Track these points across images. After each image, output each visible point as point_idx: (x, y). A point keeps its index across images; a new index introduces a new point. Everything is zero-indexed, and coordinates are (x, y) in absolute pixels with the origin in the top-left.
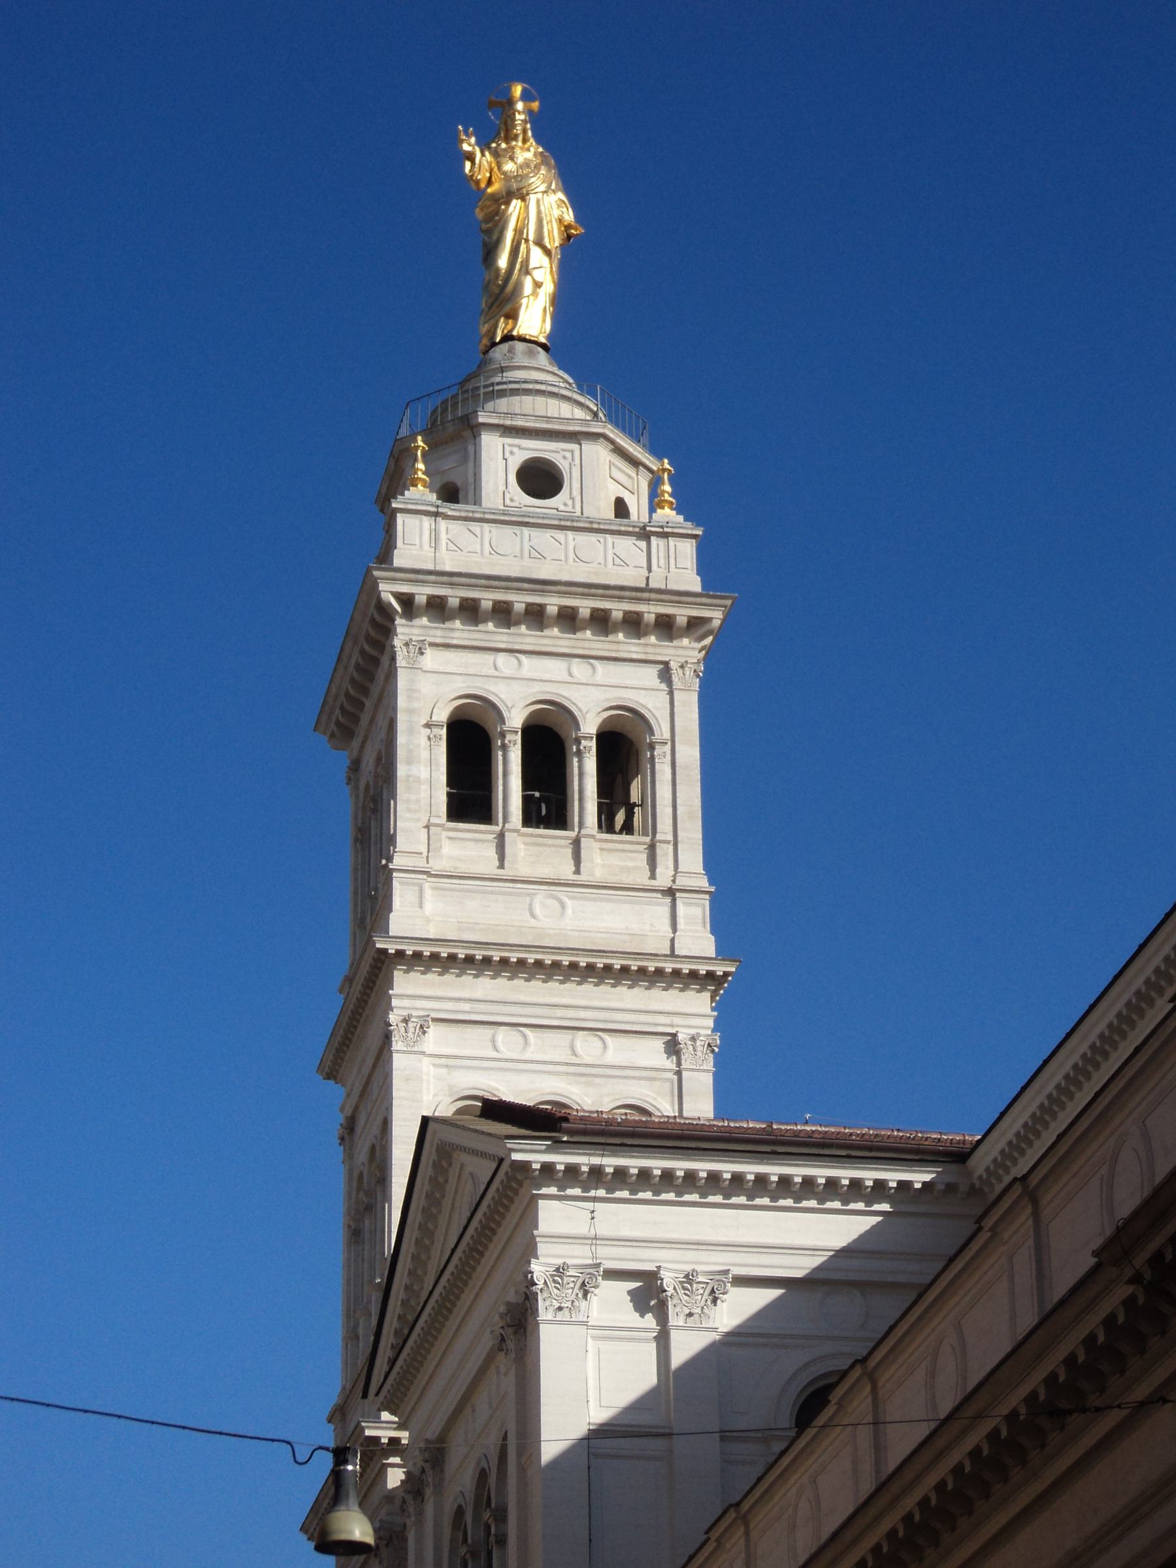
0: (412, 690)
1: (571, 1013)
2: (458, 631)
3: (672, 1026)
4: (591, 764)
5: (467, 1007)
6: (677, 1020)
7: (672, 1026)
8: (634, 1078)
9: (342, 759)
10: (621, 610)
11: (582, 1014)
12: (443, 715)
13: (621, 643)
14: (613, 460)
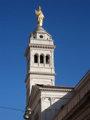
2: (35, 48)
4: (45, 58)
9: (26, 58)
12: (34, 55)
13: (48, 49)
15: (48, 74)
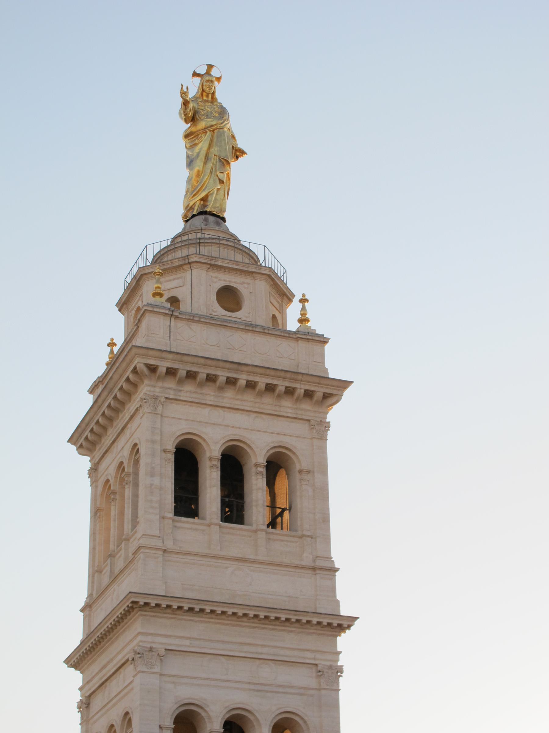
0: (154, 428)
1: (253, 649)
3: (315, 659)
5: (187, 642)
6: (318, 656)
7: (315, 659)
8: (290, 693)
10: (284, 386)
11: (260, 650)
12: (171, 446)
14: (271, 292)
15: (191, 610)
